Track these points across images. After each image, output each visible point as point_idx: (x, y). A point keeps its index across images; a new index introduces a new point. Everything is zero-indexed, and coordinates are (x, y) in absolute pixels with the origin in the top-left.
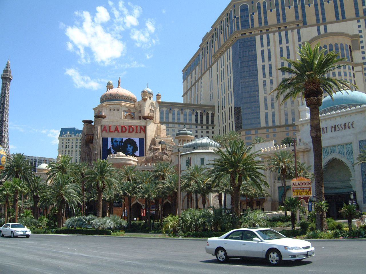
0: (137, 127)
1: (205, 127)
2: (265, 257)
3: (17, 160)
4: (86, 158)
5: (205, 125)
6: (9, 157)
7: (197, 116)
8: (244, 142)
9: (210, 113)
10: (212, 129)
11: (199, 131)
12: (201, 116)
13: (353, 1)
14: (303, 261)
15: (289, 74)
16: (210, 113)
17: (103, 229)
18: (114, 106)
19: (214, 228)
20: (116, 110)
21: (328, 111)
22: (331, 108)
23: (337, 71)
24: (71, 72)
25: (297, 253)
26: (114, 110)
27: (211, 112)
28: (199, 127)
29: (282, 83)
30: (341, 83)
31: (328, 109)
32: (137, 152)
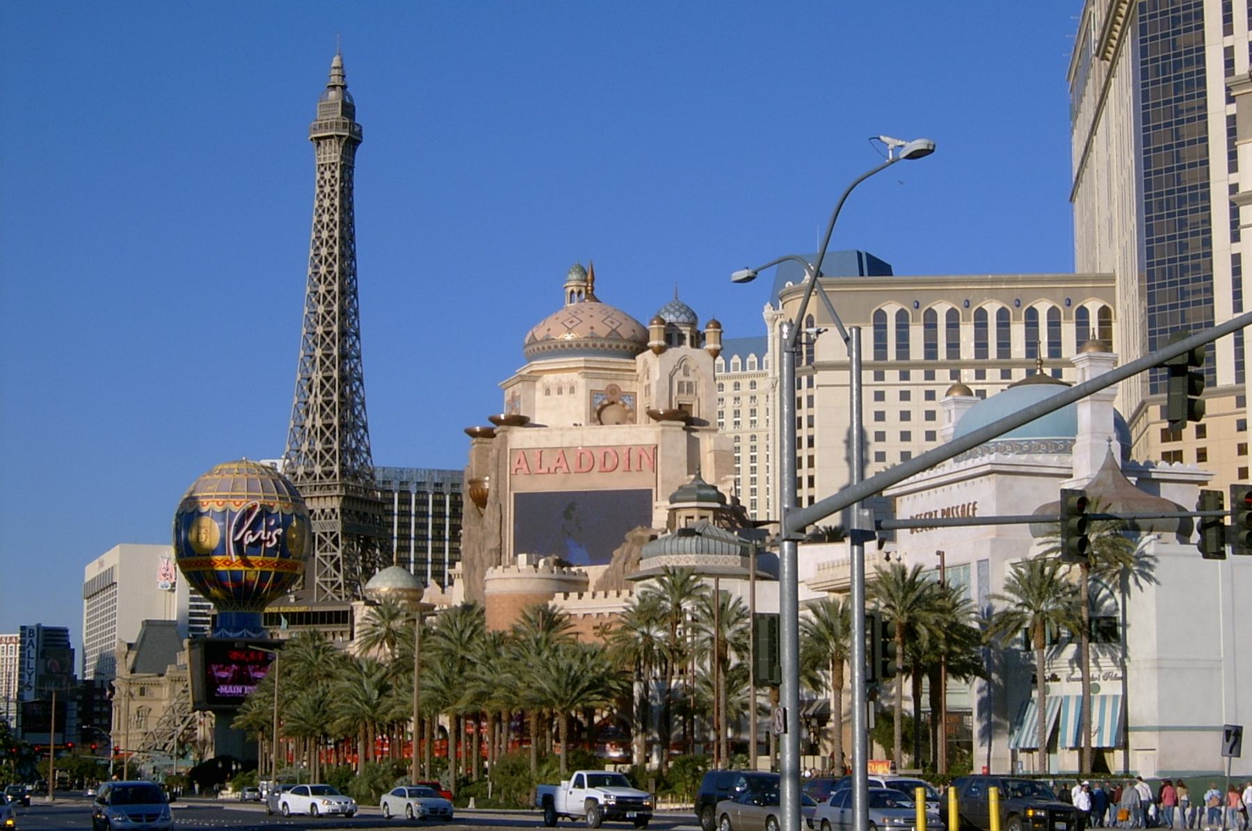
0: (1245, 412)
1: (917, 375)
2: (898, 518)
3: (579, 674)
4: (476, 563)
5: (917, 366)
6: (363, 509)
7: (930, 326)
8: (144, 731)
9: (1093, 307)
10: (923, 381)
11: (918, 394)
12: (1054, 325)
13: (1250, 774)
14: (206, 762)
15: (1078, 697)
16: (1093, 307)
17: (1125, 574)
18: (560, 375)
19: (741, 524)
20: (566, 391)
21: (1030, 447)
22: (1044, 442)
23: (322, 156)
24: (692, 806)
25: (1019, 413)
26: (560, 392)
27: (1100, 304)
28: (892, 376)
29: (799, 712)
30: (548, 772)
31: (1065, 440)
32: (1184, 431)
